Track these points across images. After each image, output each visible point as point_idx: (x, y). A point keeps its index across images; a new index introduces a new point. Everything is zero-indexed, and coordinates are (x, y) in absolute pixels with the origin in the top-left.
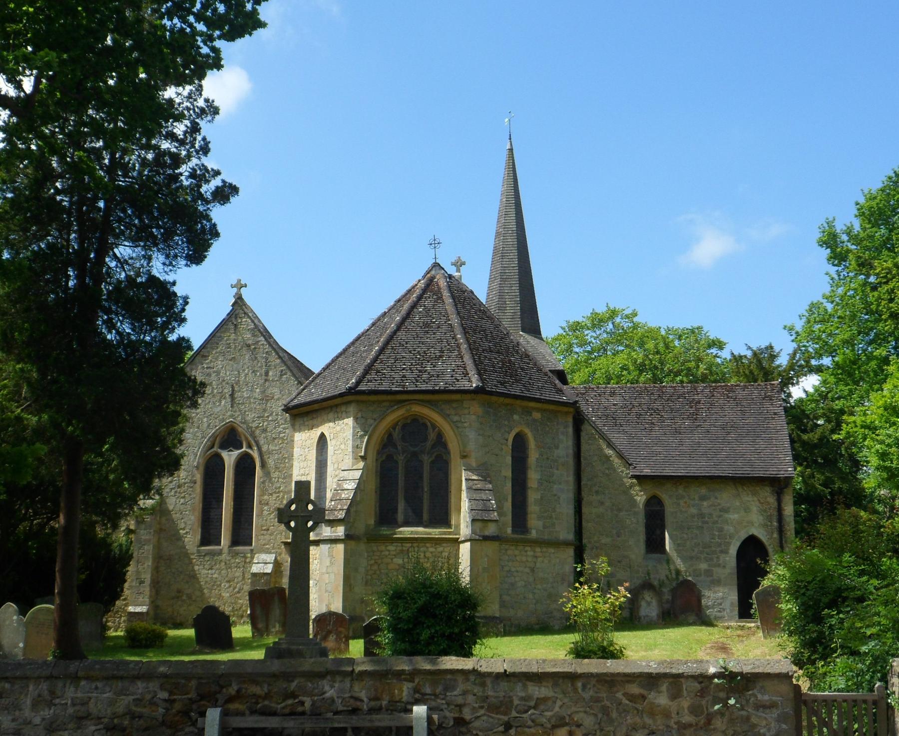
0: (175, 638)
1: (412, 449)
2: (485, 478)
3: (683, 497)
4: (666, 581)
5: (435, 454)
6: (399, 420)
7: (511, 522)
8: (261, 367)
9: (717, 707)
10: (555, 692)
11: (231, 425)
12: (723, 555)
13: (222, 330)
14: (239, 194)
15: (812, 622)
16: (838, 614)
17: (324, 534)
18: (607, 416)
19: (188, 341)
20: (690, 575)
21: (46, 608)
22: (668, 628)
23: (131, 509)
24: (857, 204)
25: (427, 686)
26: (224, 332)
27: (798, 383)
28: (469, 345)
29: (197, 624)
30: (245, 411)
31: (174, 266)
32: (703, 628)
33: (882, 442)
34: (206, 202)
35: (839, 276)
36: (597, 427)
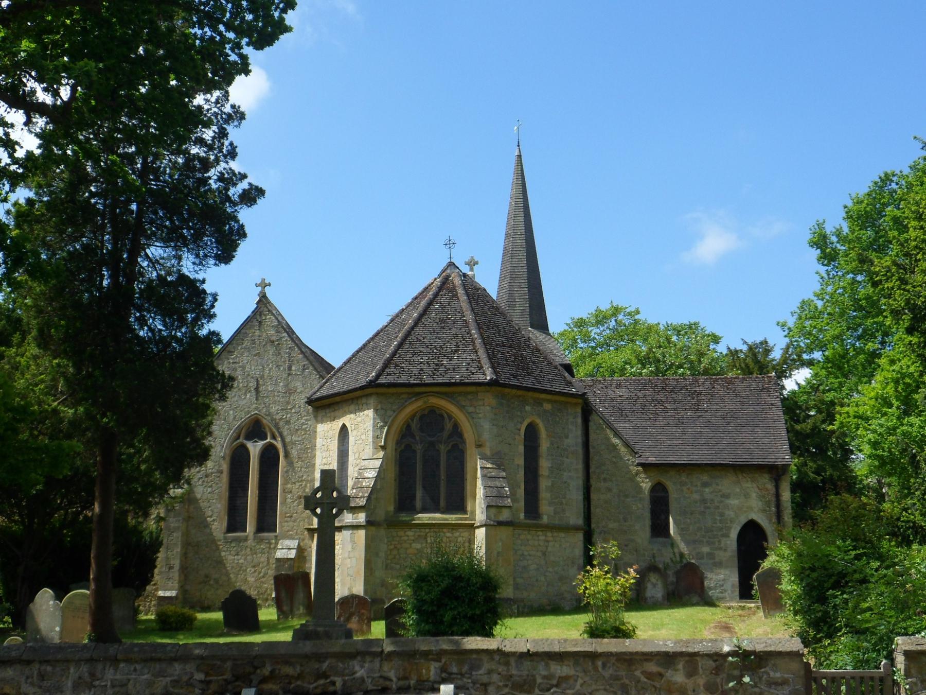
0: (203, 621)
2: (499, 466)
4: (671, 564)
5: (451, 444)
8: (284, 362)
9: (731, 684)
10: (577, 671)
11: (256, 417)
13: (248, 327)
14: (266, 195)
15: (817, 603)
16: (842, 594)
17: (346, 521)
18: (614, 407)
20: (693, 558)
21: (82, 594)
22: (673, 608)
24: (846, 207)
25: (454, 664)
26: (250, 328)
27: (790, 376)
28: (483, 339)
30: (269, 404)
31: (204, 266)
33: (874, 431)
35: (829, 275)
36: (605, 418)
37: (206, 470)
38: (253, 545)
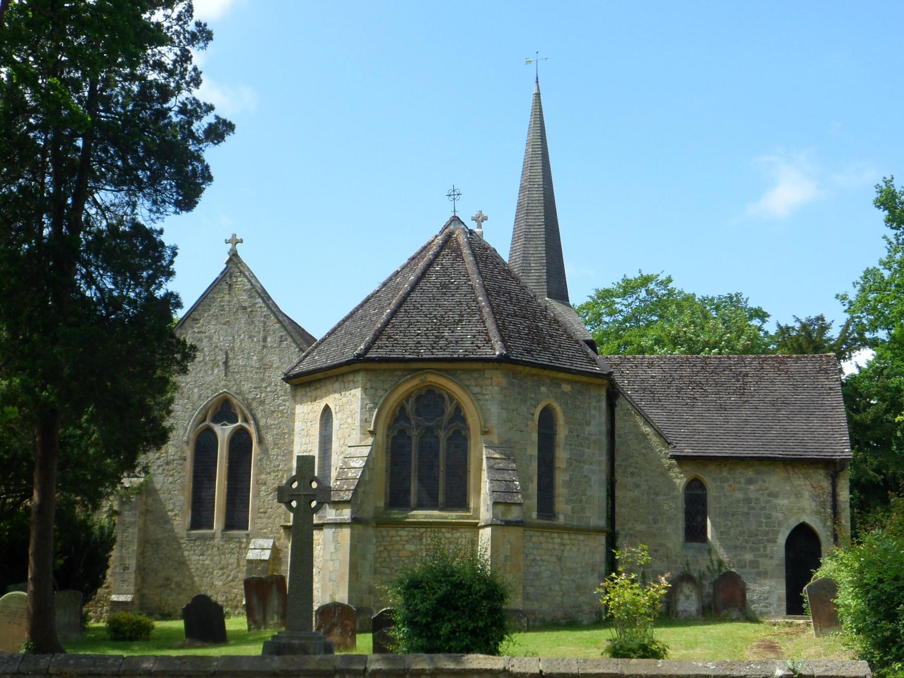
0: (162, 630)
1: (427, 424)
2: (508, 457)
3: (727, 480)
6: (412, 392)
7: (536, 505)
8: (259, 332)
12: (771, 545)
14: (235, 131)
17: (328, 517)
19: (177, 296)
20: (733, 567)
23: (114, 487)
27: (850, 357)
28: (492, 308)
29: (187, 614)
30: (241, 381)
31: (161, 213)
32: (748, 624)
34: (198, 141)
35: (898, 240)
36: (634, 402)
37: (167, 457)
38: (221, 543)
